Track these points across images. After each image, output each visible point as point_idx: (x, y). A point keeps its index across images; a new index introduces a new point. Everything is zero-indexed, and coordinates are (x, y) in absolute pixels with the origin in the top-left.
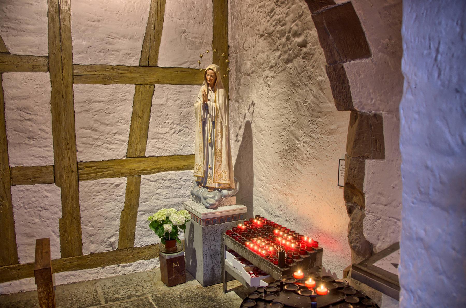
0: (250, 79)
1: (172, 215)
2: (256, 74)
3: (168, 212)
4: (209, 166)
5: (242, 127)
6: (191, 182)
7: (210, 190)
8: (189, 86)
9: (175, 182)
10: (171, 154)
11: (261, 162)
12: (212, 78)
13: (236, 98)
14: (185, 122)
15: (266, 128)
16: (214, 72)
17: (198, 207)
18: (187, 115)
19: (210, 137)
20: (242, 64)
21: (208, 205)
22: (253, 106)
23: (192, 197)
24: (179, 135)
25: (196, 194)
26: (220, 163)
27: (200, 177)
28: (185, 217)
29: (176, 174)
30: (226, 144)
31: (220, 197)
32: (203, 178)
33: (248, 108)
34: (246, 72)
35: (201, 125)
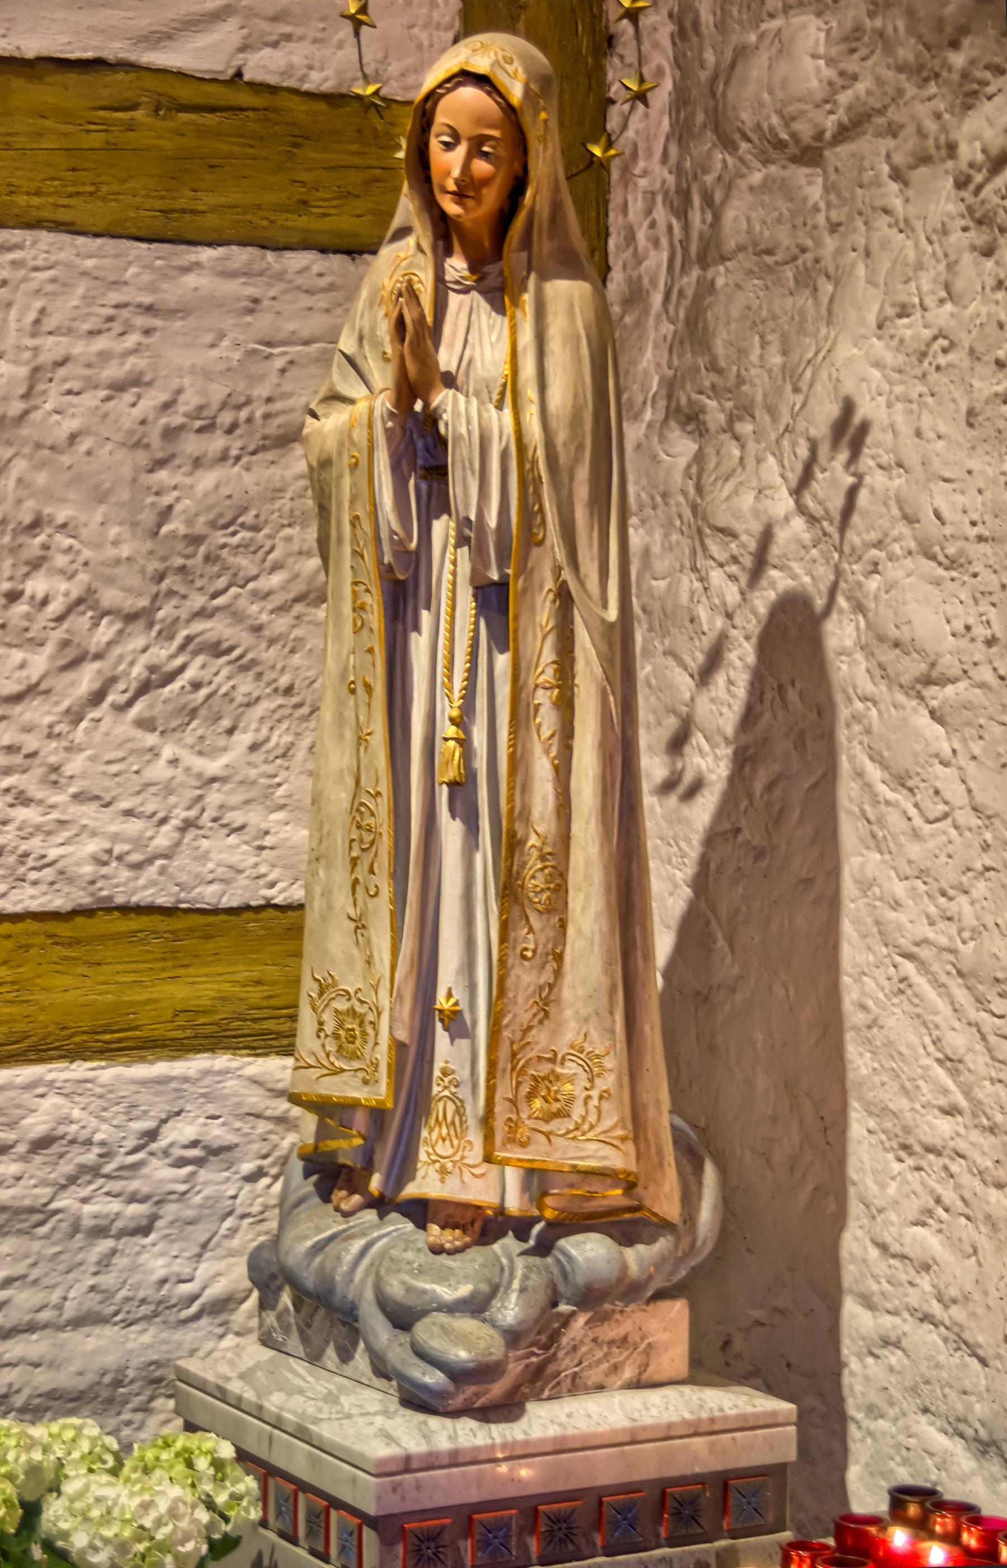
0: (815, 192)
1: (70, 1488)
2: (887, 144)
3: (37, 1456)
4: (442, 1001)
5: (732, 656)
6: (247, 1167)
7: (450, 1238)
8: (241, 256)
9: (94, 1171)
10: (58, 903)
11: (920, 981)
12: (481, 167)
13: (670, 387)
14: (198, 601)
15: (979, 652)
16: (509, 110)
17: (331, 1398)
18: (220, 537)
19: (452, 731)
20: (742, 52)
21: (434, 1378)
22: (843, 456)
23: (263, 1305)
24: (145, 724)
25: (310, 1281)
26: (547, 976)
27: (351, 1106)
28: (210, 1505)
29: (110, 1087)
30: (605, 793)
31: (542, 1297)
32: (378, 1115)
33: (794, 478)
34: (788, 121)
35: (375, 618)
